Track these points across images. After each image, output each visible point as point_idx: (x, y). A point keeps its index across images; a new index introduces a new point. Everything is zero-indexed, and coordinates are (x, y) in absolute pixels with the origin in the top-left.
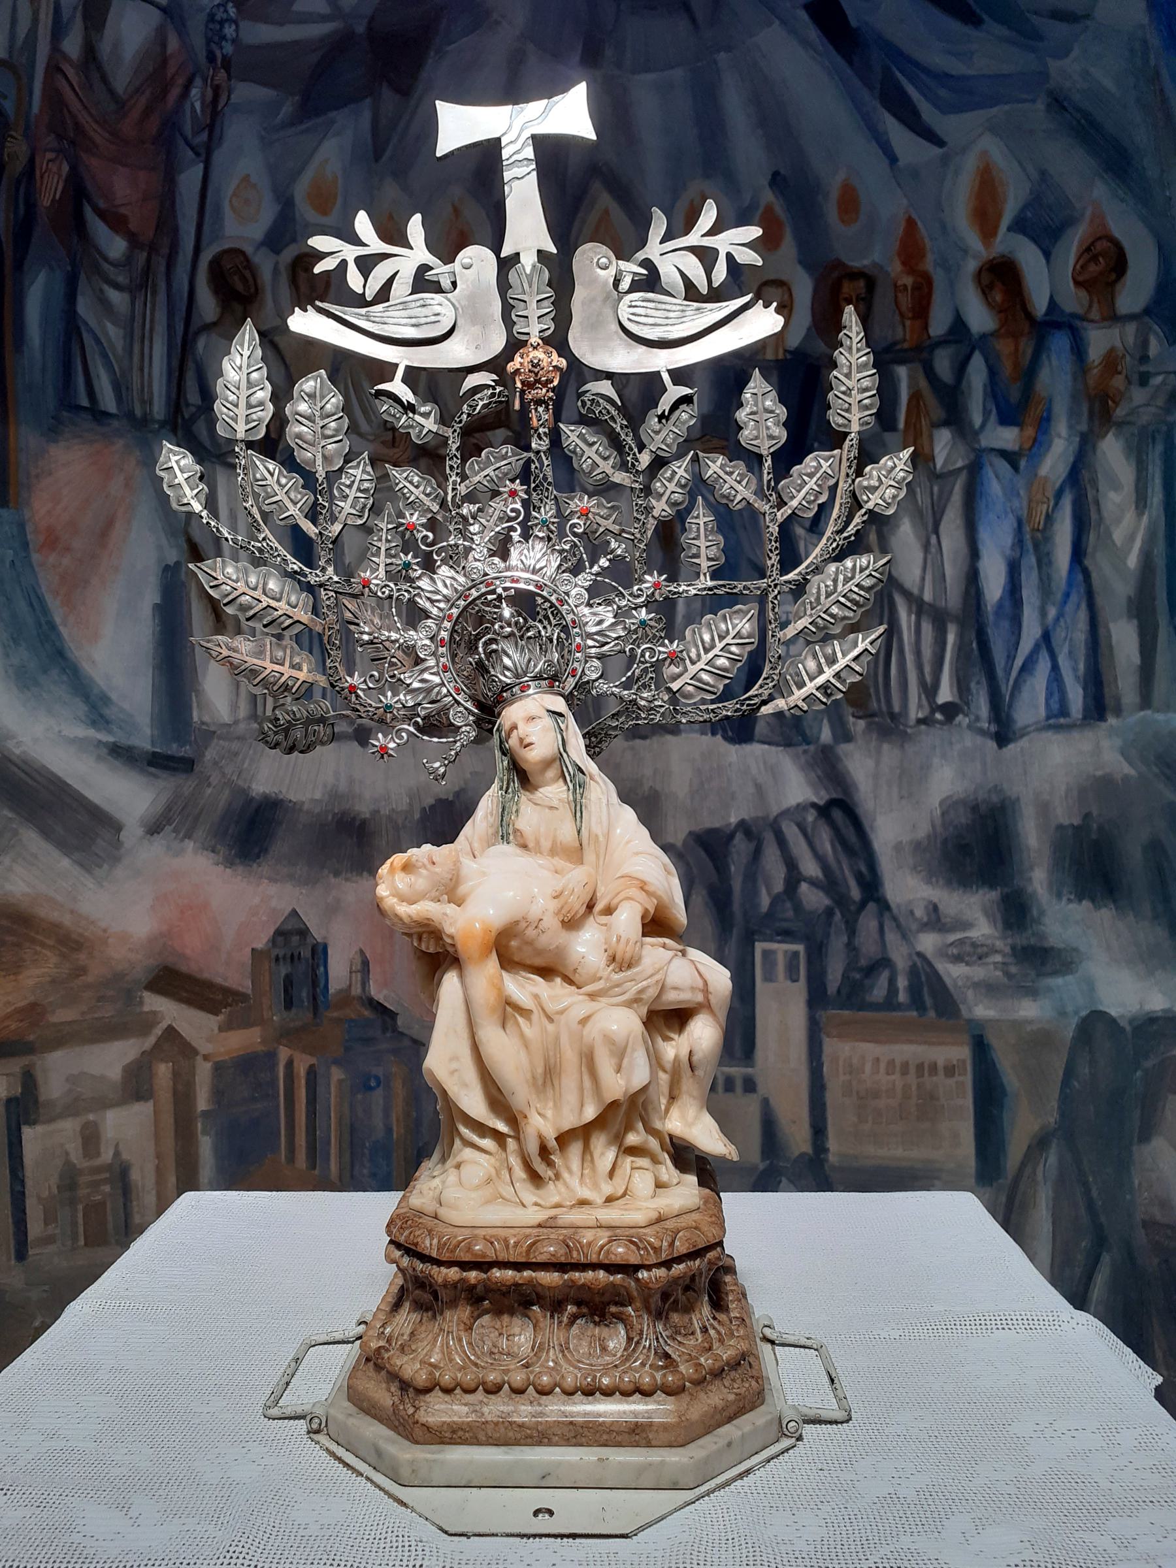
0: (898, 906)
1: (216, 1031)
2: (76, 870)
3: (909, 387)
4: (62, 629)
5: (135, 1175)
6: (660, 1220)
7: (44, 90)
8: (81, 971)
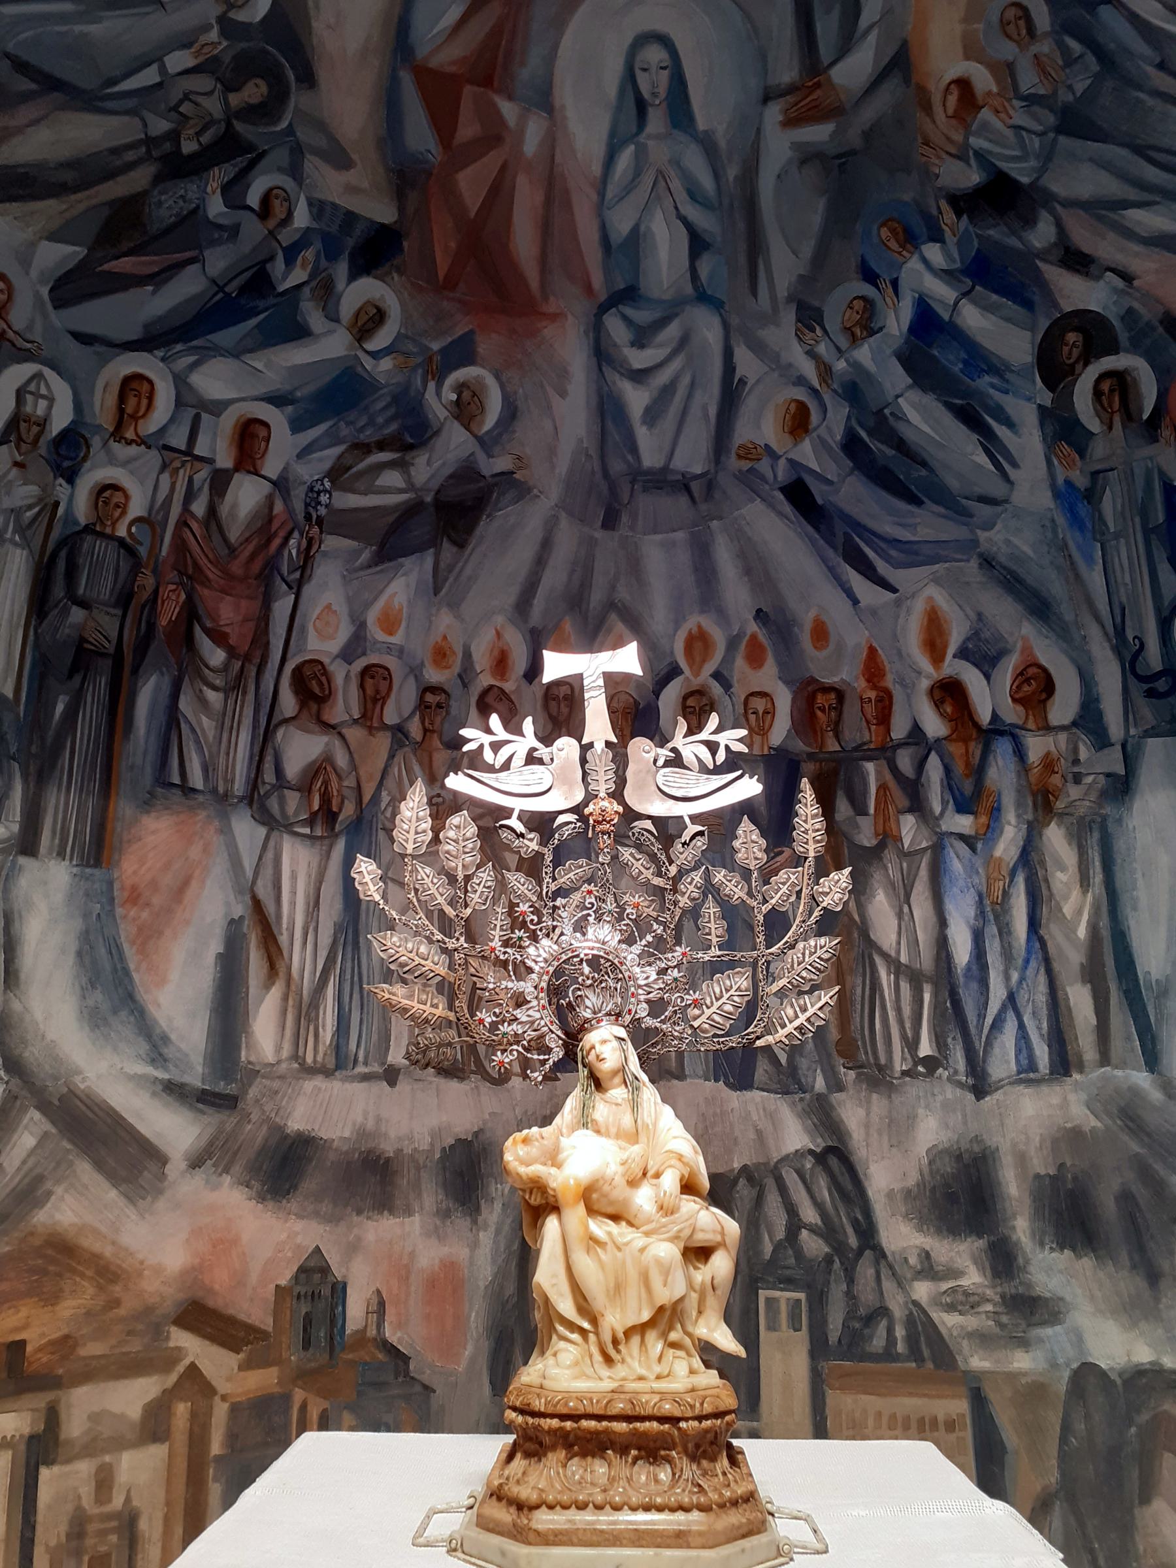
0: (893, 1253)
1: (236, 1370)
2: (122, 1202)
3: (877, 780)
4: (135, 976)
5: (143, 1525)
6: (693, 1390)
7: (173, 538)
8: (116, 1303)
